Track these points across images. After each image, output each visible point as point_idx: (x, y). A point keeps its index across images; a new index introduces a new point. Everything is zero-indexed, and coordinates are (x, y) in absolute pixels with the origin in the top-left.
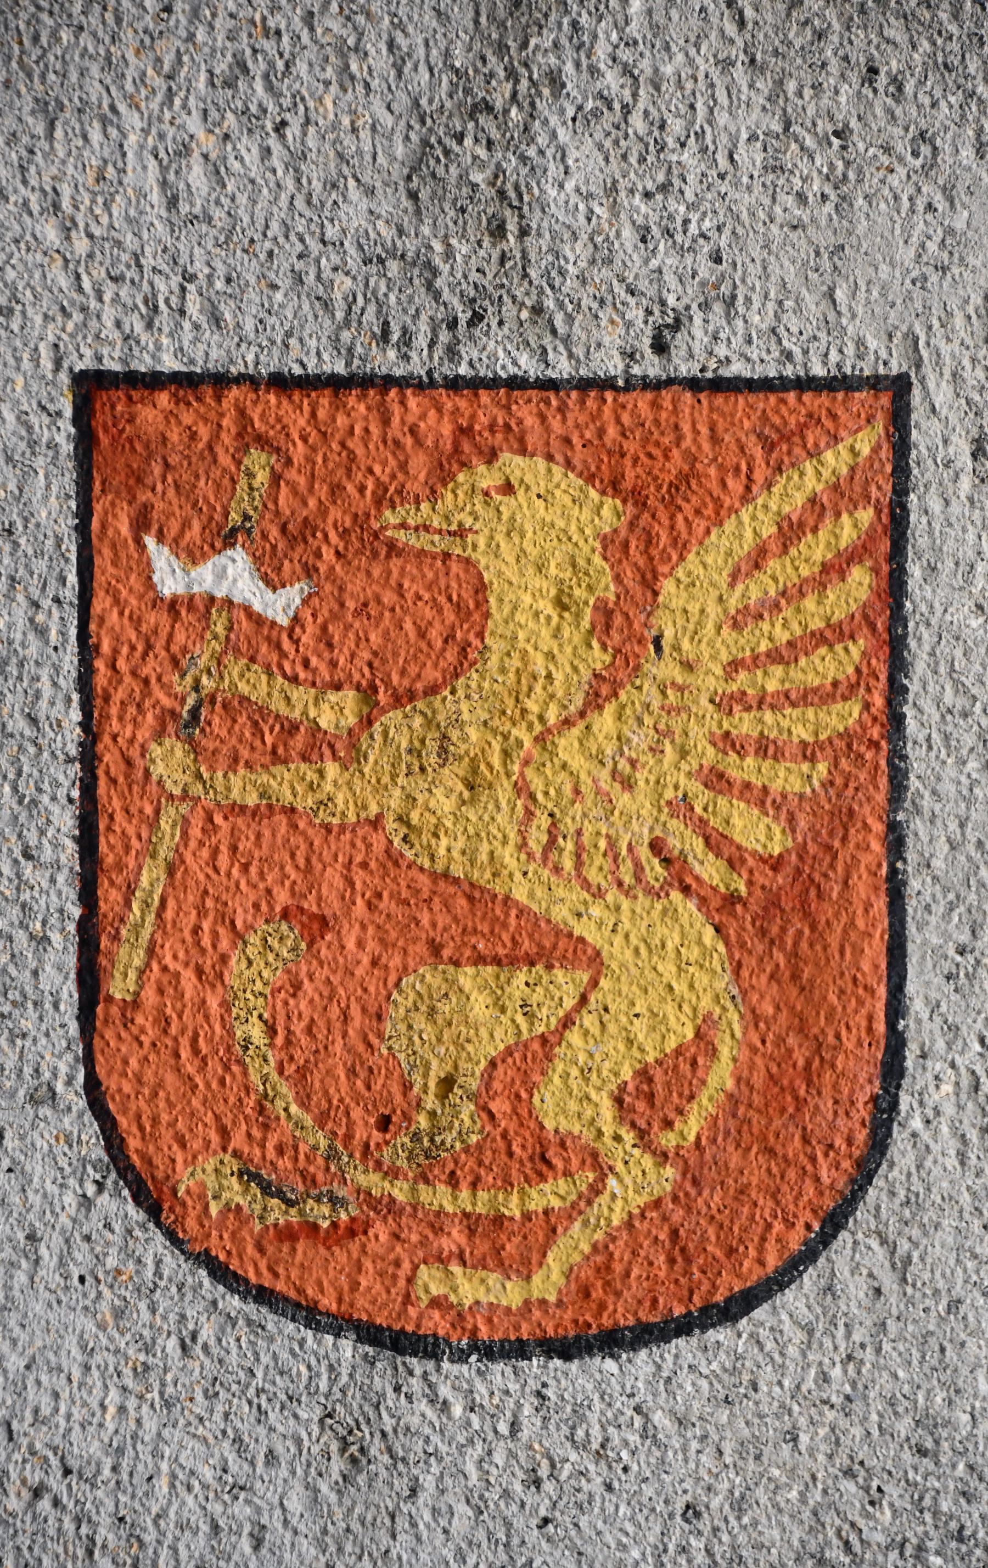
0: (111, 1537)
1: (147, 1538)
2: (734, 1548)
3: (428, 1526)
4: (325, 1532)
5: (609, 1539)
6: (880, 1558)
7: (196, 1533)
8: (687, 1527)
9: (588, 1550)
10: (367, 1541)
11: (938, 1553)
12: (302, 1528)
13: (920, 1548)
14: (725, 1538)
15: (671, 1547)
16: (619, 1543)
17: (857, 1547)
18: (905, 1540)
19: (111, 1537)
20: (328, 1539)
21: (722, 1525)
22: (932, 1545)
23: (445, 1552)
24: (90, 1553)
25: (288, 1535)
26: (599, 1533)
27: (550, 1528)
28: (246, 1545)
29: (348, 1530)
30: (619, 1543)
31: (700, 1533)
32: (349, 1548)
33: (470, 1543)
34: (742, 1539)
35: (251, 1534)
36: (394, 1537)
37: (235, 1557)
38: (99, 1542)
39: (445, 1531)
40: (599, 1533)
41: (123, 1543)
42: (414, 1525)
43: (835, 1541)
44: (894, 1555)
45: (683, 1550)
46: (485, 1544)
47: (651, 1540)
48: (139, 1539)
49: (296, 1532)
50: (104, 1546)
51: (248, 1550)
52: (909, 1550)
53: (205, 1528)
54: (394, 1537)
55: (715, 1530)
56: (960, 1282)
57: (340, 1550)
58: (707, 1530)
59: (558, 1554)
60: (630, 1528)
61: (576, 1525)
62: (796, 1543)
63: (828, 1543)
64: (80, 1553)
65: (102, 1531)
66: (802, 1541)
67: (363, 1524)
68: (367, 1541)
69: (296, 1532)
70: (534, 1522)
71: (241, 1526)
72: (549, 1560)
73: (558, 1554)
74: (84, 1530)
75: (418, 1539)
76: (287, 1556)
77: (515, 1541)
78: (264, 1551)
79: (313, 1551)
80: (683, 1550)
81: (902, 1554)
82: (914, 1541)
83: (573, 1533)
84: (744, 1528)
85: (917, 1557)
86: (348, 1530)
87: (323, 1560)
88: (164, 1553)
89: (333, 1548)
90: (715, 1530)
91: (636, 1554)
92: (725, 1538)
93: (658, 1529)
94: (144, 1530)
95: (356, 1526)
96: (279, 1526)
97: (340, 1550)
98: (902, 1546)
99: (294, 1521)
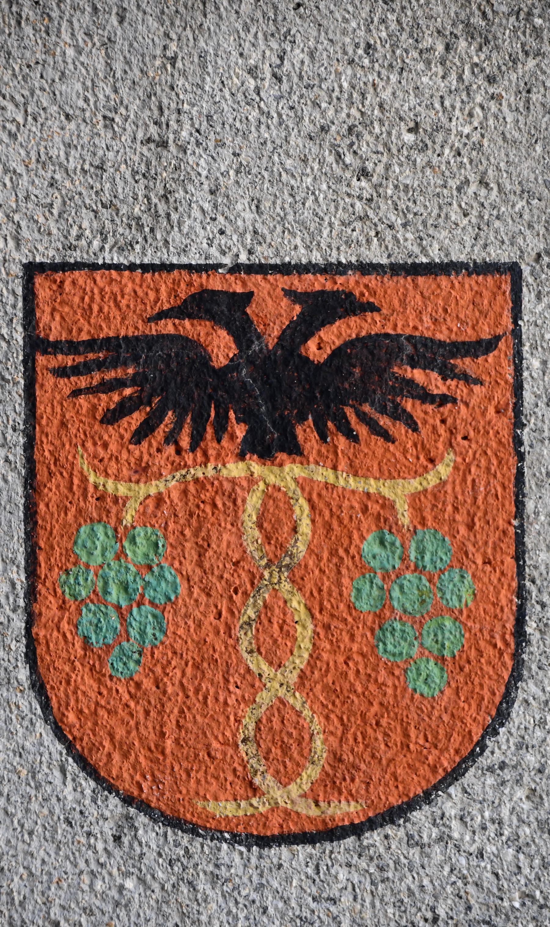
0: (31, 13)
1: (53, 15)
2: (414, 19)
3: (226, 9)
4: (163, 13)
5: (337, 15)
6: (504, 21)
7: (83, 13)
8: (385, 7)
9: (325, 22)
10: (189, 19)
11: (540, 16)
12: (148, 10)
13: (529, 14)
14: (409, 13)
15: (376, 20)
16: (344, 18)
17: (490, 15)
18: (520, 9)
19: (31, 13)
20: (165, 17)
21: (408, 5)
22: (536, 12)
23: (237, 25)
24: (19, 23)
25: (140, 14)
26: (331, 12)
27: (302, 9)
28: (114, 20)
29: (177, 11)
30: (344, 18)
31: (394, 11)
32: (178, 22)
33: (252, 19)
34: (419, 13)
35: (117, 14)
36: (205, 16)
37: (108, 27)
38: (24, 17)
39: (237, 12)
40: (331, 12)
41: (39, 17)
42: (217, 8)
43: (477, 12)
44: (513, 19)
45: (383, 21)
46: (261, 20)
47: (364, 15)
48: (48, 15)
49: (145, 13)
50: (27, 19)
51: (116, 23)
52: (522, 15)
53: (89, 9)
54: (205, 16)
55: (403, 8)
56: (34, 159)
57: (172, 24)
58: (398, 9)
59: (306, 25)
60: (351, 9)
61: (317, 7)
62: (453, 14)
63: (472, 14)
64: (13, 23)
65: (26, 9)
66: (456, 13)
67: (186, 8)
68: (189, 19)
69: (145, 13)
70: (291, 6)
71: (111, 9)
72: (301, 29)
73: (306, 25)
74: (14, 9)
75: (220, 17)
76: (140, 27)
77: (280, 18)
78: (126, 24)
79: (156, 24)
80: (383, 21)
81: (517, 18)
82: (526, 9)
83: (315, 12)
84: (421, 6)
85: (527, 20)
86: (177, 11)
87: (162, 30)
88: (65, 24)
89: (168, 23)
90: (403, 8)
91: (354, 24)
92: (409, 13)
93: (368, 9)
94: (52, 9)
95: (182, 9)
96: (134, 9)
97: (172, 24)
98: (518, 13)
99: (144, 6)
